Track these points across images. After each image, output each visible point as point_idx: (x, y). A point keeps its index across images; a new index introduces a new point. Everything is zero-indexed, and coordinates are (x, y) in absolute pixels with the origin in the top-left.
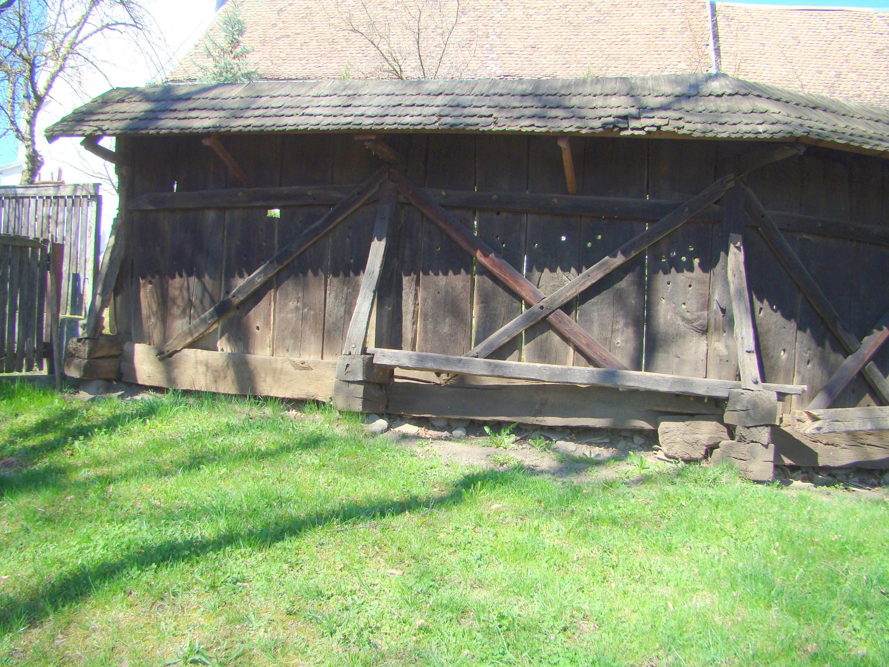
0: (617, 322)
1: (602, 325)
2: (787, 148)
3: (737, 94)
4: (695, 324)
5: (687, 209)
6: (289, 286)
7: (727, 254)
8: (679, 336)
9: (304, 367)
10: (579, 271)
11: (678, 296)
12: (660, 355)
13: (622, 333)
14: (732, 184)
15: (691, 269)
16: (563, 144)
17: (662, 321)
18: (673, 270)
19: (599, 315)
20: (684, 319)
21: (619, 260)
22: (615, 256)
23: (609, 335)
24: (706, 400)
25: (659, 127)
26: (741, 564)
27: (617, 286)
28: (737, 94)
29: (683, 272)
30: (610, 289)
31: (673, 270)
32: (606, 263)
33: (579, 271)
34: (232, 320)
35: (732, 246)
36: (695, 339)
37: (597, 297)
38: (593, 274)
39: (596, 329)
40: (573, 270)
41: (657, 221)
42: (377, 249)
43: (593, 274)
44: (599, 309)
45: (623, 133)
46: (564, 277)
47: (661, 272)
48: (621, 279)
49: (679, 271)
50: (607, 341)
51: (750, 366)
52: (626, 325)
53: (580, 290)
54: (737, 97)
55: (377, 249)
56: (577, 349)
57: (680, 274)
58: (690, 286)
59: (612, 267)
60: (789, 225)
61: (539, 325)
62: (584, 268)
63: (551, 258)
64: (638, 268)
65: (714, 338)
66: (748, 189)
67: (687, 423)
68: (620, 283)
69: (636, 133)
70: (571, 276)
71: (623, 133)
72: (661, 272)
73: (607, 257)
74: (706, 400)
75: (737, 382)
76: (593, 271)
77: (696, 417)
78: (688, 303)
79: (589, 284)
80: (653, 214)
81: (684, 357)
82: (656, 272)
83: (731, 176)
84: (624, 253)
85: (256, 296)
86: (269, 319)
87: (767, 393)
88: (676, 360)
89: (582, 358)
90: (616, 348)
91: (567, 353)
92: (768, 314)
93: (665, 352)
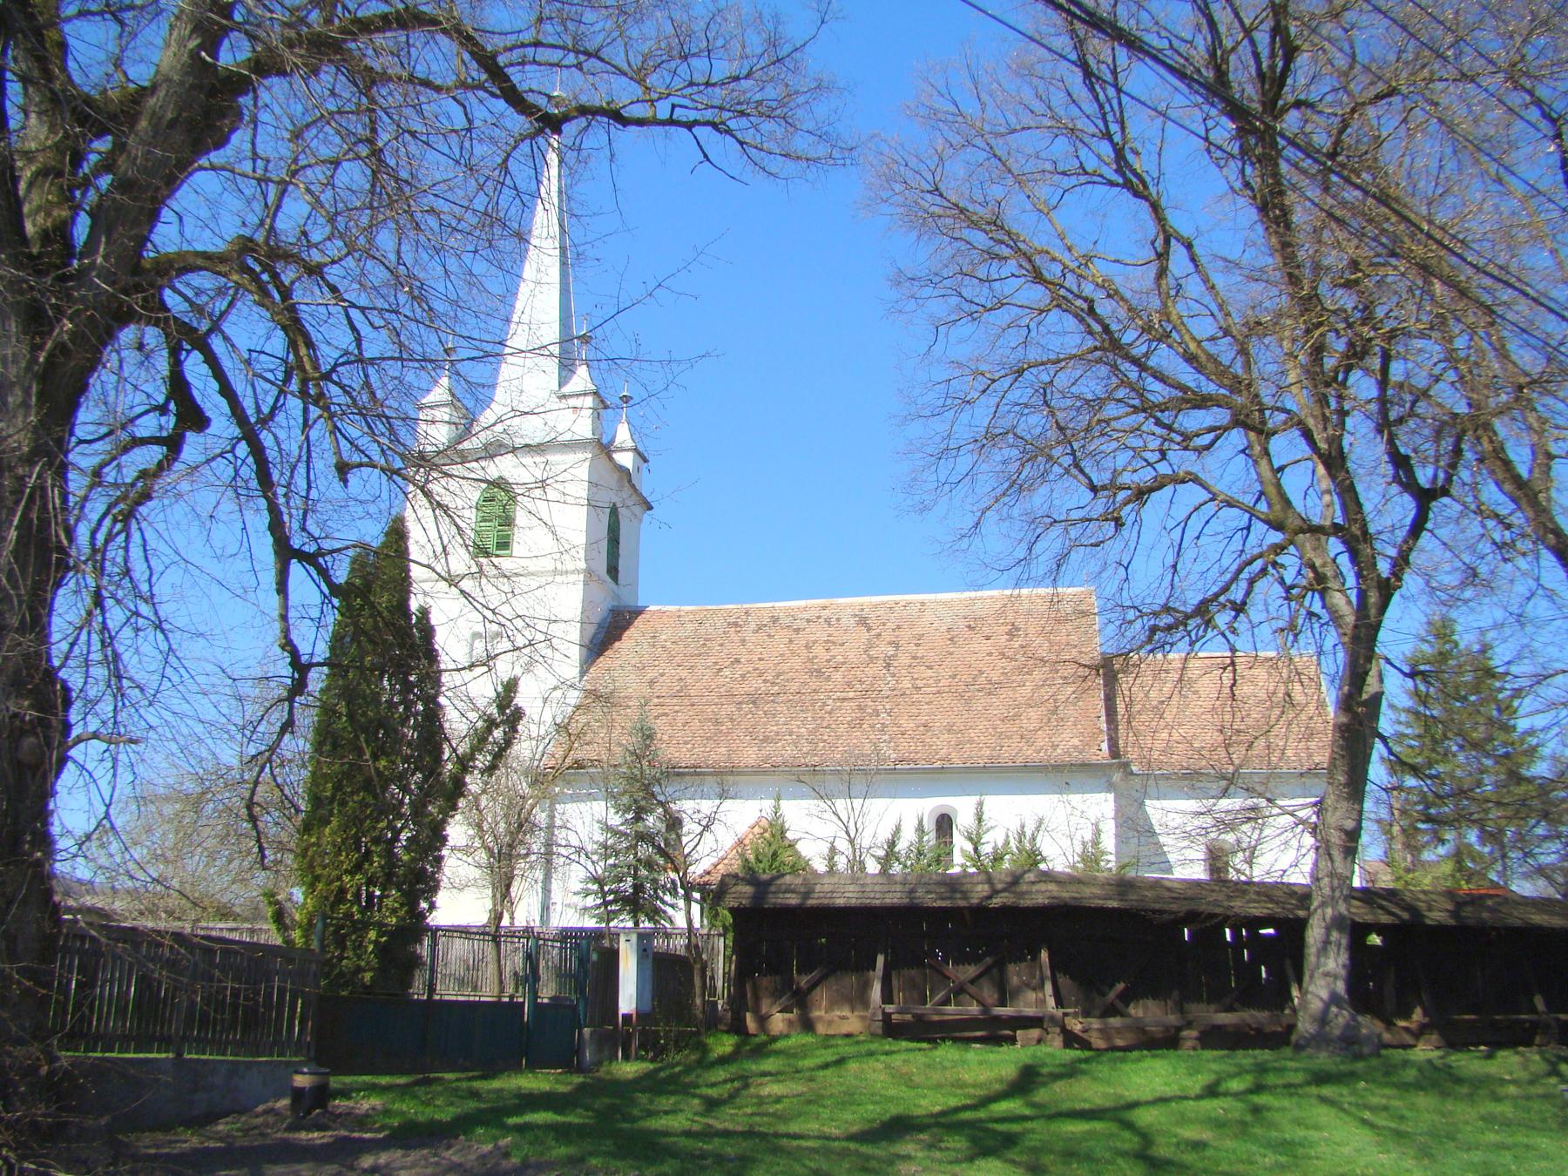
6: (832, 980)
9: (843, 1018)
11: (1016, 974)
24: (1325, 975)
26: (1540, 831)
34: (800, 1001)
42: (880, 960)
44: (984, 982)
51: (1051, 1002)
55: (880, 960)
61: (960, 990)
63: (962, 959)
74: (1325, 975)
85: (814, 986)
86: (822, 996)
87: (1059, 1012)
92: (1063, 980)
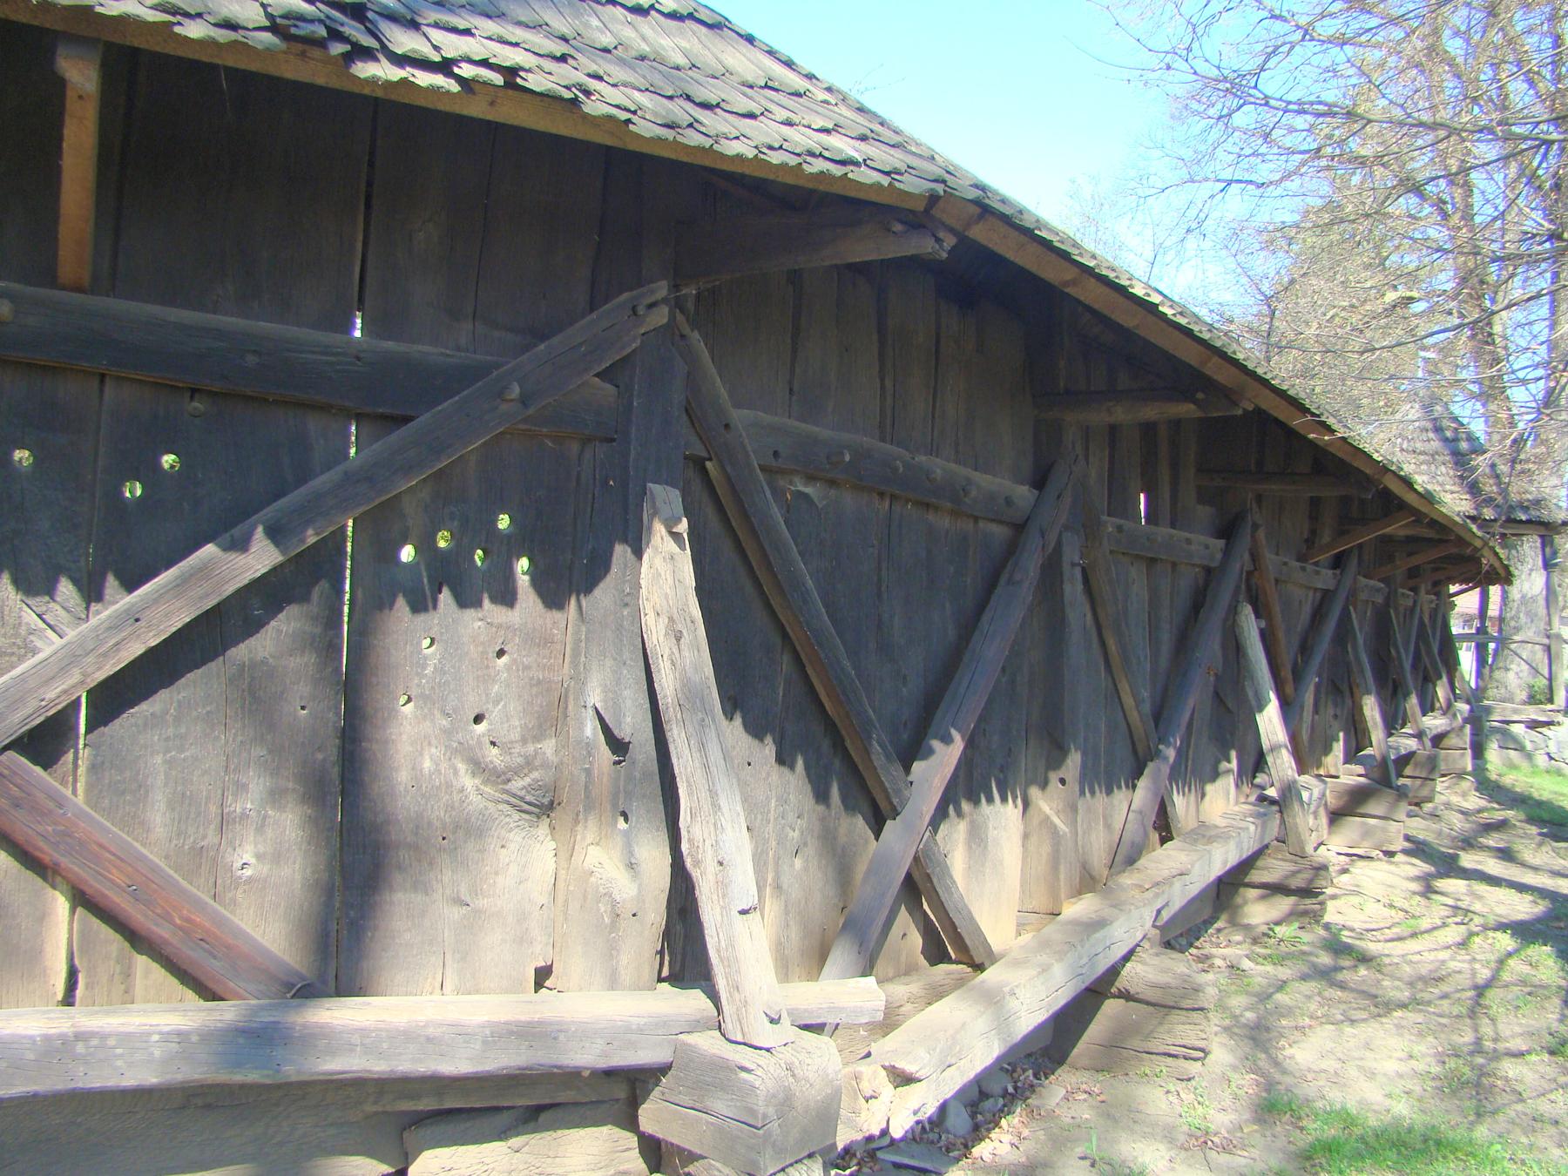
0: (241, 788)
1: (183, 802)
2: (898, 227)
3: (691, 16)
4: (517, 785)
5: (515, 391)
7: (639, 553)
8: (467, 831)
10: (92, 593)
11: (467, 685)
12: (399, 896)
13: (260, 829)
14: (660, 317)
15: (506, 596)
16: (81, 76)
17: (403, 777)
18: (445, 596)
19: (170, 763)
20: (479, 767)
21: (261, 557)
22: (240, 545)
23: (212, 838)
25: (511, 72)
27: (241, 652)
28: (691, 16)
29: (478, 604)
30: (213, 666)
31: (445, 596)
32: (204, 570)
33: (92, 593)
35: (659, 529)
36: (516, 838)
37: (163, 695)
38: (159, 607)
39: (158, 816)
40: (66, 588)
41: (406, 420)
43: (159, 607)
45: (366, 70)
46: (30, 617)
47: (401, 603)
48: (252, 627)
49: (466, 600)
50: (204, 860)
52: (275, 797)
53: (101, 676)
54: (690, 24)
56: (82, 899)
57: (470, 614)
58: (501, 653)
59: (230, 589)
60: (776, 454)
62: (111, 583)
64: (319, 590)
65: (588, 832)
66: (696, 335)
67: (516, 1141)
68: (252, 642)
69: (424, 79)
70: (56, 612)
71: (366, 70)
72: (401, 603)
73: (210, 549)
75: (693, 1001)
76: (157, 599)
77: (543, 1117)
78: (494, 714)
79: (136, 649)
80: (387, 399)
81: (482, 903)
82: (383, 603)
83: (661, 289)
84: (276, 534)
88: (456, 913)
89: (105, 931)
90: (236, 882)
91: (42, 917)
93: (415, 887)
